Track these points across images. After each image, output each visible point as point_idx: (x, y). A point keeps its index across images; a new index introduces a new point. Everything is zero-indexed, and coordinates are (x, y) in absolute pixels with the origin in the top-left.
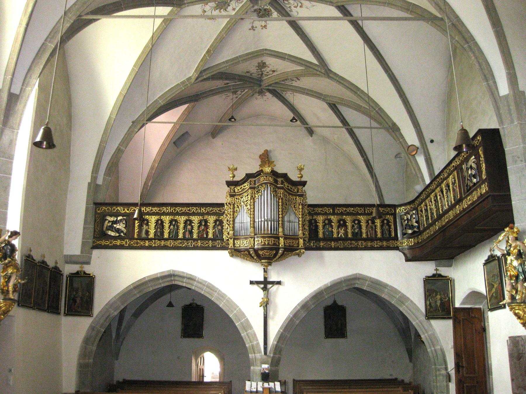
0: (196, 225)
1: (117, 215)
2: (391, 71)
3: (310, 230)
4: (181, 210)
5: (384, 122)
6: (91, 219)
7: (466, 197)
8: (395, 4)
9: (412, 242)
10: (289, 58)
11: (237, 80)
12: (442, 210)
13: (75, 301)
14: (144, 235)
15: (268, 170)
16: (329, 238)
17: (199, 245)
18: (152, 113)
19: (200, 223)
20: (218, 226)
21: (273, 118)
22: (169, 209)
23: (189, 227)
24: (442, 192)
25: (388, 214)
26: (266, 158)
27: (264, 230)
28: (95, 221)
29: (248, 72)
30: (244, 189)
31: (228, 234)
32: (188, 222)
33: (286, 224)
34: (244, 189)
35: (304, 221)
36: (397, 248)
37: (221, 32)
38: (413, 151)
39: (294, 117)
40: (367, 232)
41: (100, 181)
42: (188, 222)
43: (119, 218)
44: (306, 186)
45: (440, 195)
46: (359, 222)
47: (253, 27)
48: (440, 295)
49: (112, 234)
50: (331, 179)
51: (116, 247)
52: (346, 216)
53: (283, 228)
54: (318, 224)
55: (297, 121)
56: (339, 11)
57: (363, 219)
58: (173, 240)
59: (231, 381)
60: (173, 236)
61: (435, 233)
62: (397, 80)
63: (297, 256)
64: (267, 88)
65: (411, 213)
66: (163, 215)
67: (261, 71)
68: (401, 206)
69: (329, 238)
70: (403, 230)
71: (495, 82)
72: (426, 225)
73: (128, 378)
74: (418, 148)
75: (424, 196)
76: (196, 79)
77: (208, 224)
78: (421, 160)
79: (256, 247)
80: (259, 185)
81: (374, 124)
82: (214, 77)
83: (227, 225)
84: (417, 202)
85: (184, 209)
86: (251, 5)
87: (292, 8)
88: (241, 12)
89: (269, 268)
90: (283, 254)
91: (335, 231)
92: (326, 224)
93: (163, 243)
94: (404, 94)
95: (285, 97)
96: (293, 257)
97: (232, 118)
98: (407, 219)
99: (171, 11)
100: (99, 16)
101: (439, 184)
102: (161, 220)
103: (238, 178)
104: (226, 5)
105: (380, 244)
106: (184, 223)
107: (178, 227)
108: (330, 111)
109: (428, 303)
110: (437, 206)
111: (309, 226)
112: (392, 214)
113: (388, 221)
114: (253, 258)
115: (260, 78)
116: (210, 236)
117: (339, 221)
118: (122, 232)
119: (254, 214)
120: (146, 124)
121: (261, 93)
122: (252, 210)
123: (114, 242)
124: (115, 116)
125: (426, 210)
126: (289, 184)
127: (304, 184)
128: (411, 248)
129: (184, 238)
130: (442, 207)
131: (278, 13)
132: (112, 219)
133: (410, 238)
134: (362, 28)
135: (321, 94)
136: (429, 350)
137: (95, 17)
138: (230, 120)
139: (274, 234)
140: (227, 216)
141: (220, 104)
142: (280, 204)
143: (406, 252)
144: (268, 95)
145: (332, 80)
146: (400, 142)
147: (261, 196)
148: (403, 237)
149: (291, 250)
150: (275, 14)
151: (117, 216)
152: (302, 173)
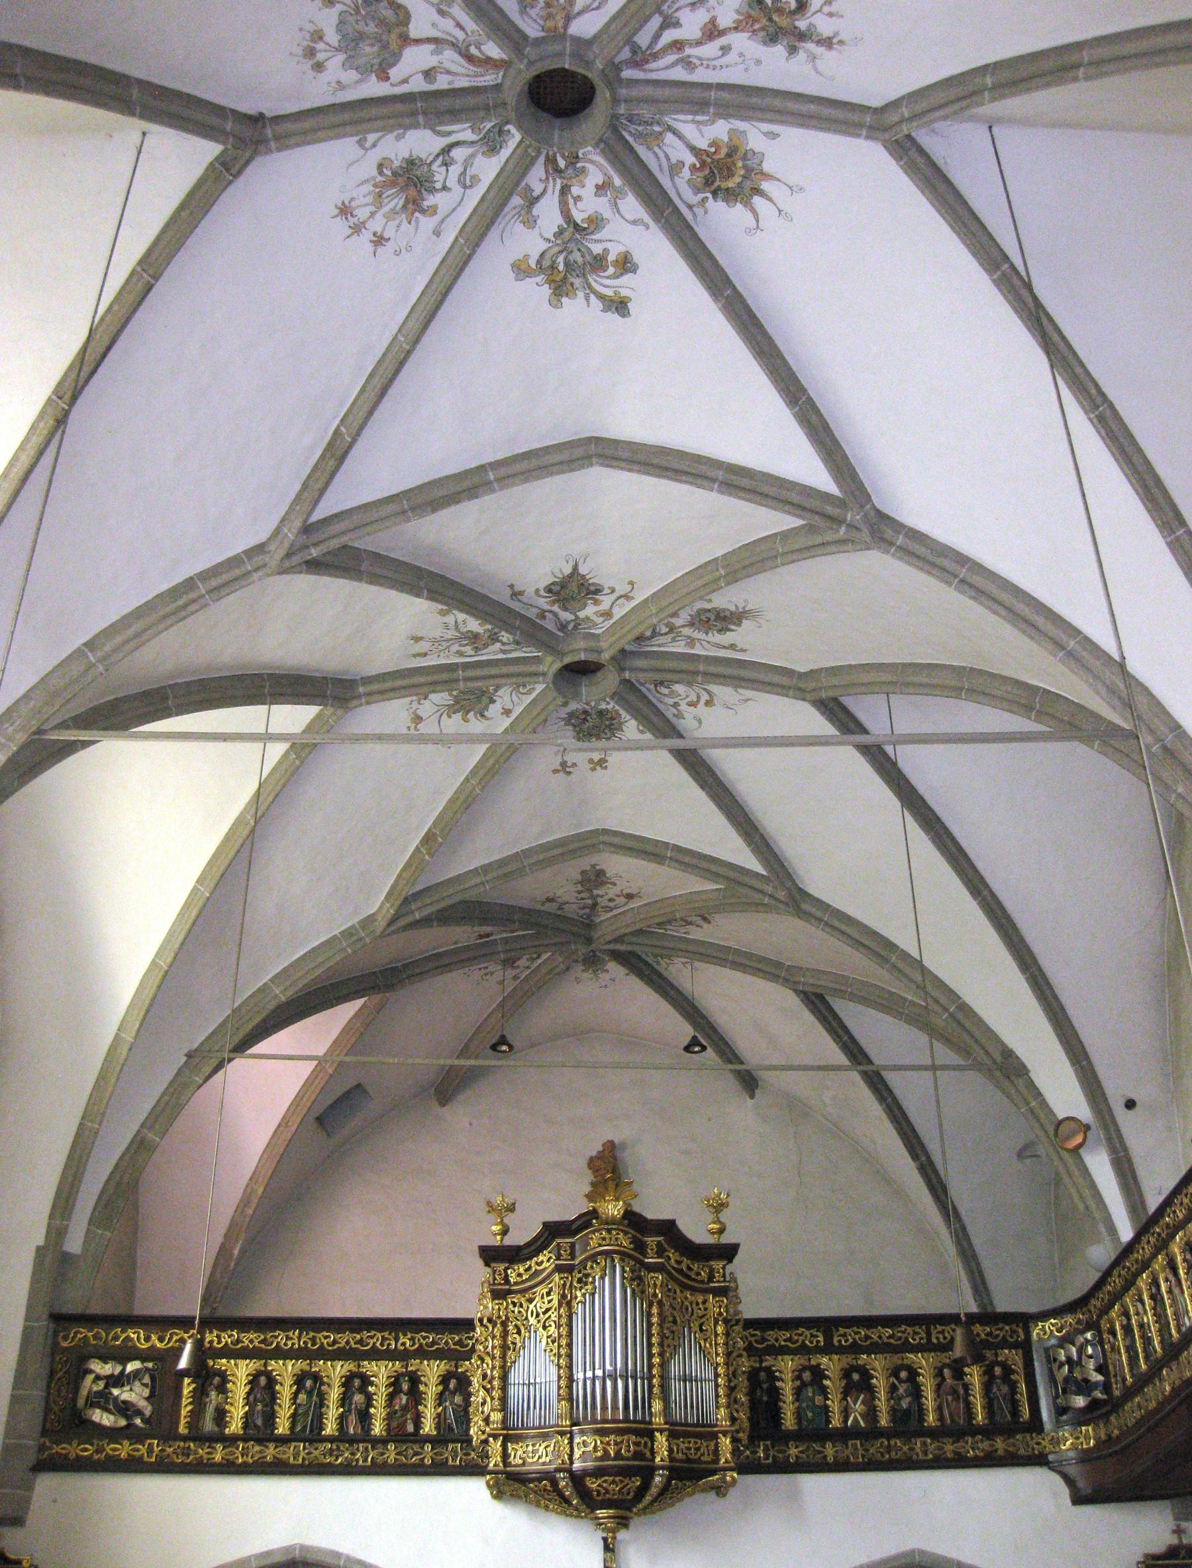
0: (380, 1391)
1: (124, 1354)
2: (991, 892)
3: (754, 1405)
4: (335, 1342)
5: (975, 1047)
6: (38, 1367)
8: (987, 691)
9: (1089, 1435)
11: (516, 925)
12: (1178, 1327)
14: (209, 1425)
15: (613, 1209)
16: (815, 1431)
17: (391, 1460)
18: (251, 1026)
19: (395, 1383)
20: (454, 1393)
21: (629, 1040)
23: (358, 1398)
24: (1174, 1269)
25: (1004, 1344)
26: (608, 1169)
27: (604, 1408)
28: (52, 1374)
29: (550, 900)
30: (537, 1273)
31: (487, 1420)
32: (357, 1383)
33: (676, 1387)
34: (537, 1273)
35: (732, 1376)
36: (1039, 1460)
37: (467, 780)
38: (1073, 1134)
39: (694, 1038)
41: (74, 1244)
42: (357, 1383)
43: (131, 1367)
44: (736, 1260)
45: (1167, 1280)
46: (913, 1374)
47: (564, 764)
50: (819, 1247)
52: (869, 1354)
53: (666, 1399)
54: (778, 1384)
55: (704, 1048)
56: (823, 714)
57: (924, 1363)
58: (304, 1440)
60: (304, 1429)
61: (1161, 1405)
62: (1008, 918)
63: (712, 1495)
64: (611, 947)
65: (1080, 1339)
66: (276, 1358)
67: (593, 897)
68: (1044, 1316)
69: (815, 1431)
70: (1057, 1396)
72: (1129, 1380)
74: (1087, 1128)
75: (1115, 1282)
76: (389, 925)
77: (422, 1388)
78: (1100, 1165)
79: (577, 1465)
80: (586, 1259)
81: (945, 1055)
82: (445, 917)
83: (482, 1393)
84: (1095, 1303)
85: (345, 1339)
86: (560, 701)
87: (683, 706)
88: (526, 721)
89: (622, 1535)
90: (665, 1489)
91: (834, 1405)
92: (804, 1385)
93: (271, 1452)
94: (1035, 961)
95: (665, 973)
96: (699, 1496)
97: (503, 1040)
99: (318, 717)
100: (95, 732)
101: (1163, 1245)
103: (519, 1237)
104: (485, 700)
105: (985, 1445)
106: (343, 1385)
107: (322, 1397)
108: (808, 1017)
110: (1160, 1317)
111: (751, 1393)
112: (1015, 1346)
113: (1007, 1370)
114: (567, 1501)
115: (589, 916)
116: (428, 1427)
117: (846, 1374)
118: (139, 1413)
119: (570, 1356)
120: (230, 1060)
121: (592, 962)
122: (564, 1342)
123: (109, 1448)
124: (134, 1033)
125: (1128, 1329)
126: (682, 1255)
127: (729, 1252)
128: (1086, 1457)
129: (342, 1437)
130: (1177, 1319)
131: (640, 723)
132: (107, 1369)
133: (1081, 1424)
134: (894, 764)
135: (778, 965)
137: (84, 736)
138: (494, 1047)
139: (635, 1421)
140: (482, 1360)
141: (461, 999)
142: (655, 1320)
143: (1072, 1471)
144: (612, 966)
146: (1032, 1111)
147: (593, 1294)
148: (1058, 1421)
149: (691, 1474)
150: (631, 729)
151: (124, 1361)
152: (725, 1216)
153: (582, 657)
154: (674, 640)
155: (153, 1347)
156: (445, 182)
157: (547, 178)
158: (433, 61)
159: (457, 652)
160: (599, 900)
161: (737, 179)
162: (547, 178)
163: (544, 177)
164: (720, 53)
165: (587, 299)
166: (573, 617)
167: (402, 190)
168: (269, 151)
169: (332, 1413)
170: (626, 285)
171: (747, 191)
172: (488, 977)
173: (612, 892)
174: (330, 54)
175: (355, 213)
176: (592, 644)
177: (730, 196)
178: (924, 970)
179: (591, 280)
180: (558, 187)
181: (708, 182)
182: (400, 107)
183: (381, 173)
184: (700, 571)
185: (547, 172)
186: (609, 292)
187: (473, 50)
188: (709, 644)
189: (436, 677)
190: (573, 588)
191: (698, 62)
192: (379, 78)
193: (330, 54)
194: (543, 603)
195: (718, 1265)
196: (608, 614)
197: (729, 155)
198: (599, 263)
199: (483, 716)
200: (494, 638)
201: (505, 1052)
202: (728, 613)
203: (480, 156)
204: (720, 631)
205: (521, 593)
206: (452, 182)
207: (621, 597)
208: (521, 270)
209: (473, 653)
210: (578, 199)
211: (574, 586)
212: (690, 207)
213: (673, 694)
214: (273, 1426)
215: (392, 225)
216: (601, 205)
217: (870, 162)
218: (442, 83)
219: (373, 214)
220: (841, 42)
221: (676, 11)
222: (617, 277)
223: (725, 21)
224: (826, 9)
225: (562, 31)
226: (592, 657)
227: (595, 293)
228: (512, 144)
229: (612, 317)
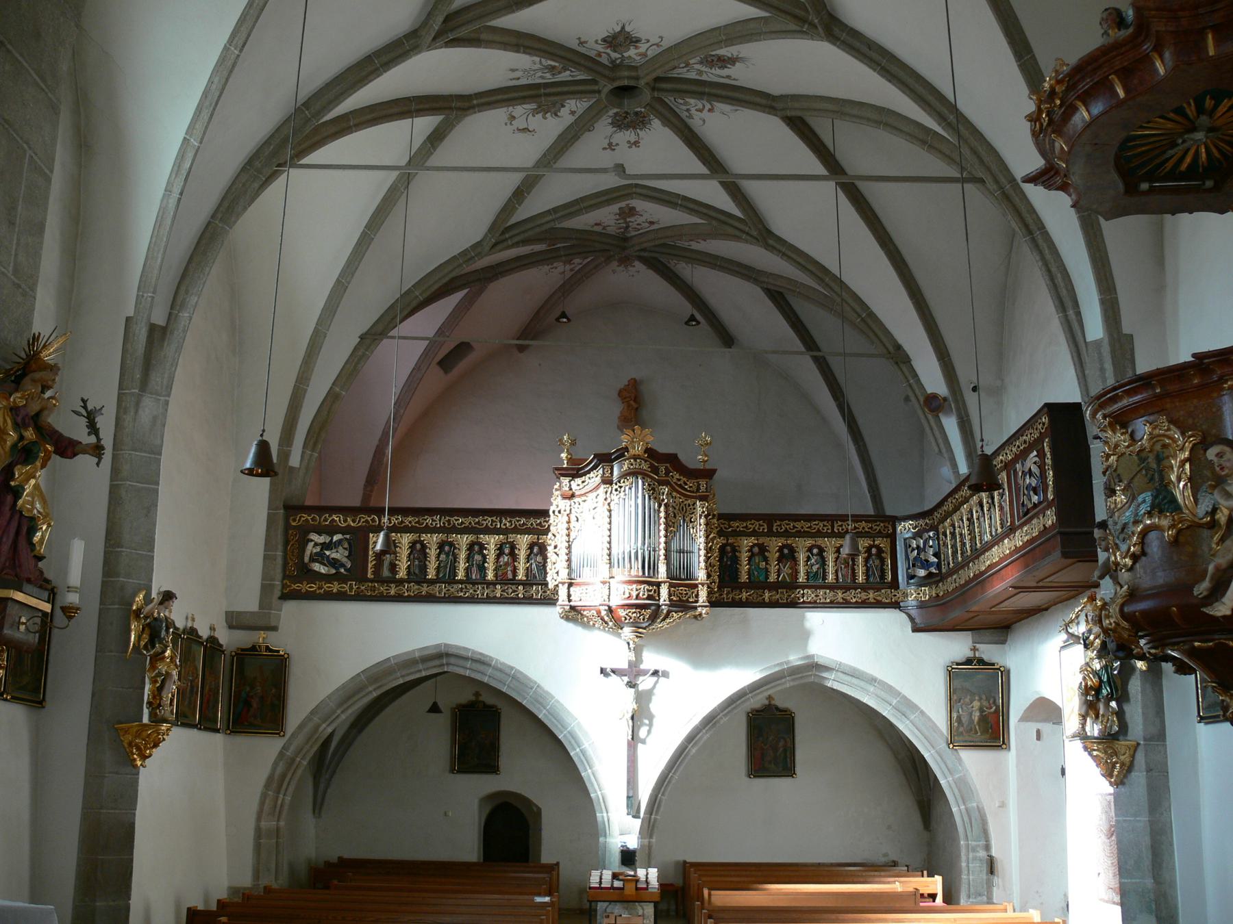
1: (331, 530)
7: (1021, 526)
9: (926, 593)
10: (684, 203)
13: (247, 703)
14: (386, 573)
17: (498, 595)
22: (438, 521)
23: (478, 557)
33: (674, 556)
36: (896, 605)
40: (836, 571)
43: (335, 538)
47: (610, 144)
48: (980, 699)
49: (323, 570)
51: (329, 597)
59: (558, 864)
65: (926, 535)
67: (626, 222)
71: (1078, 314)
73: (347, 855)
75: (948, 506)
85: (470, 521)
87: (693, 111)
91: (773, 569)
93: (425, 589)
97: (563, 315)
98: (918, 547)
102: (422, 543)
104: (558, 105)
107: (455, 557)
109: (955, 715)
110: (971, 532)
112: (887, 536)
116: (521, 576)
118: (343, 565)
121: (625, 261)
125: (953, 534)
128: (922, 605)
129: (468, 580)
132: (321, 539)
134: (833, 156)
136: (954, 809)
143: (914, 612)
144: (637, 263)
151: (331, 534)
153: (626, 83)
155: (349, 526)
169: (462, 565)
176: (633, 74)
188: (714, 75)
189: (525, 94)
190: (620, 39)
194: (600, 48)
195: (703, 483)
196: (644, 55)
200: (565, 69)
211: (621, 39)
213: (686, 104)
214: (426, 574)
226: (632, 83)
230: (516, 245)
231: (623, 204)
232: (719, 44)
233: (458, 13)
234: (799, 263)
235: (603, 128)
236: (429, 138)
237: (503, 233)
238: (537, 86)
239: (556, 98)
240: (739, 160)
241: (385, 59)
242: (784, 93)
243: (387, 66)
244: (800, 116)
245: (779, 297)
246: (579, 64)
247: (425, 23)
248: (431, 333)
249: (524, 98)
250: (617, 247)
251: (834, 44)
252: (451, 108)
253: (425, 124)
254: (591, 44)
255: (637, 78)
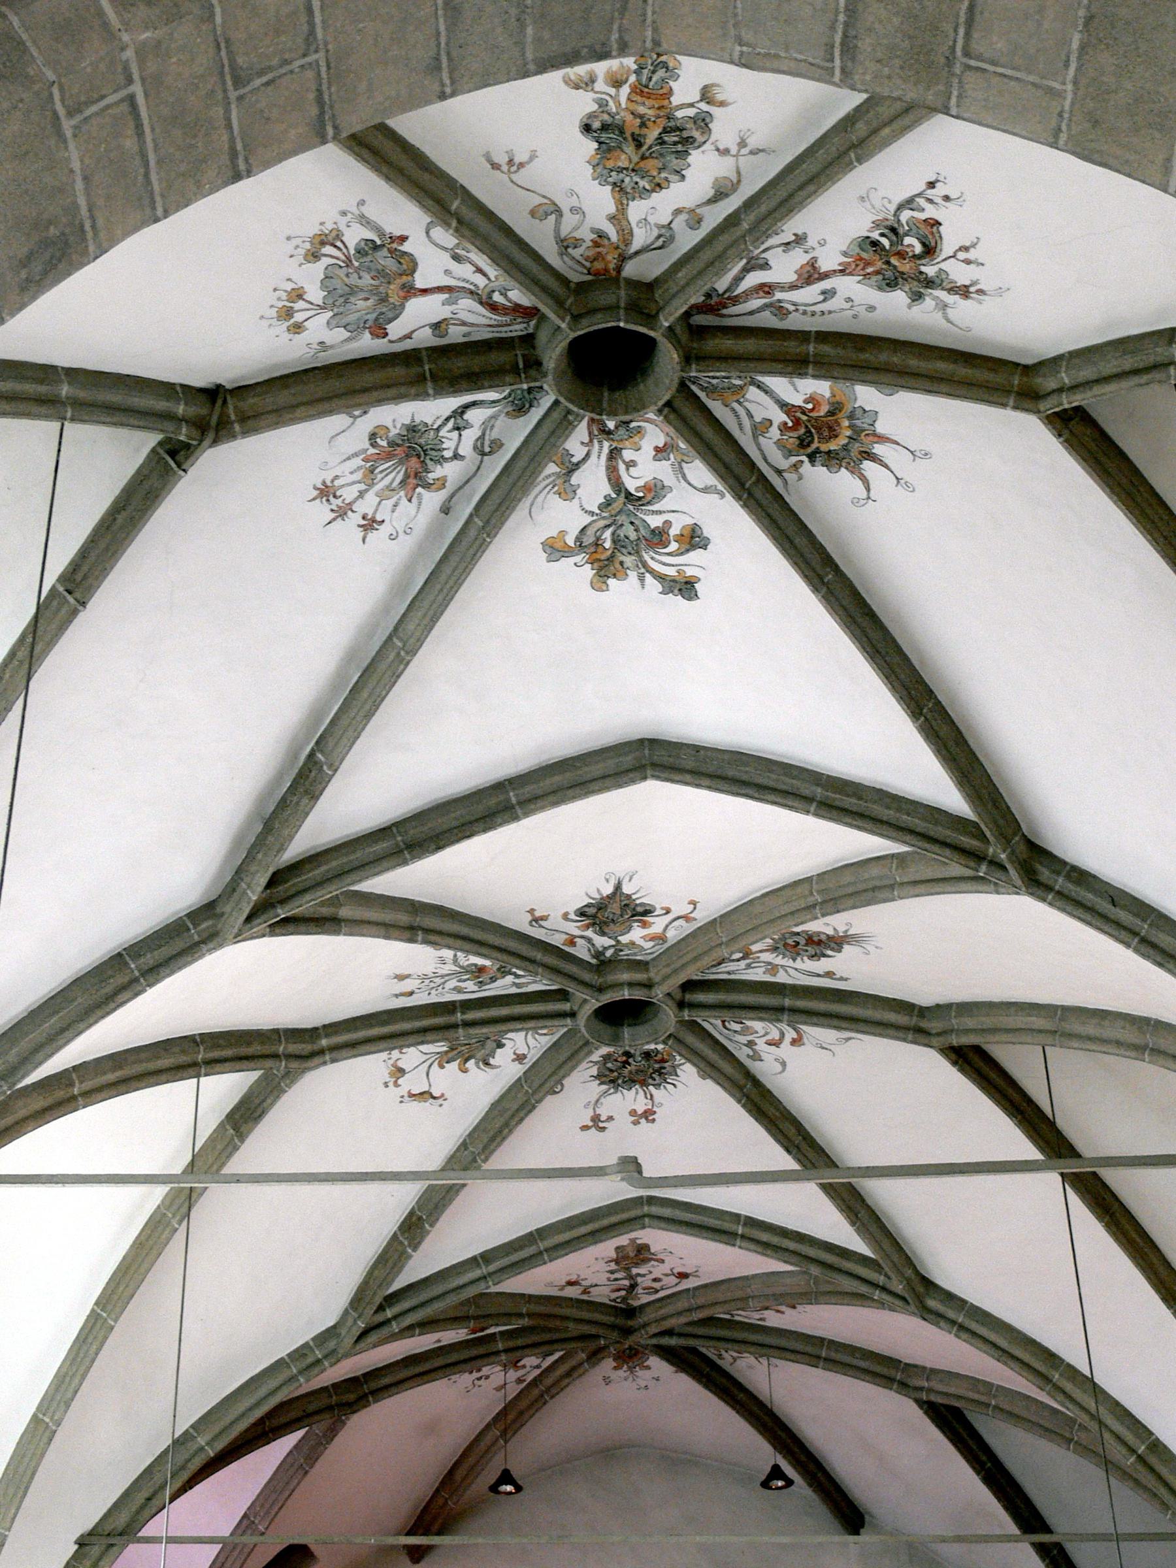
10: (748, 1231)
21: (677, 1460)
47: (596, 1119)
64: (654, 1341)
67: (631, 1277)
87: (761, 1045)
97: (506, 1477)
104: (490, 1044)
115: (624, 1299)
121: (630, 1357)
134: (1052, 1124)
144: (654, 1361)
145: (937, 1325)
153: (626, 994)
154: (749, 966)
156: (456, 449)
157: (591, 441)
158: (445, 312)
159: (455, 989)
160: (639, 1279)
161: (842, 441)
162: (591, 441)
163: (586, 440)
164: (821, 298)
165: (642, 579)
166: (613, 943)
167: (401, 462)
168: (234, 437)
170: (694, 562)
171: (854, 453)
172: (481, 1382)
173: (658, 1270)
174: (313, 312)
175: (338, 494)
176: (639, 977)
177: (832, 460)
178: (1096, 1390)
179: (646, 557)
180: (606, 450)
181: (803, 443)
182: (399, 372)
183: (374, 445)
184: (789, 892)
185: (590, 433)
186: (671, 572)
187: (497, 297)
188: (800, 971)
190: (612, 910)
191: (792, 308)
192: (375, 335)
193: (313, 312)
194: (573, 929)
196: (660, 938)
197: (831, 413)
198: (658, 538)
199: (487, 1064)
200: (503, 972)
201: (510, 1493)
202: (823, 937)
203: (502, 417)
204: (811, 957)
205: (544, 918)
206: (466, 449)
207: (679, 918)
208: (555, 549)
209: (476, 988)
210: (631, 464)
211: (615, 908)
212: (779, 472)
213: (746, 1031)
215: (388, 504)
216: (663, 471)
217: (1023, 442)
218: (456, 335)
219: (361, 494)
220: (980, 292)
221: (764, 251)
222: (682, 554)
223: (829, 261)
224: (962, 255)
225: (614, 273)
226: (639, 995)
227: (652, 572)
228: (546, 402)
229: (677, 601)
230: (409, 1331)
231: (623, 1240)
232: (810, 910)
233: (295, 867)
234: (995, 1345)
235: (581, 1087)
236: (230, 1116)
237: (381, 1308)
238: (448, 1008)
239: (485, 1030)
240: (856, 1140)
241: (149, 959)
242: (942, 1000)
243: (154, 973)
244: (974, 1043)
245: (952, 1421)
246: (532, 961)
247: (232, 888)
248: (225, 1528)
249: (425, 1030)
250: (612, 1330)
251: (1043, 900)
252: (275, 1056)
253: (223, 1089)
254: (555, 921)
255: (649, 985)
